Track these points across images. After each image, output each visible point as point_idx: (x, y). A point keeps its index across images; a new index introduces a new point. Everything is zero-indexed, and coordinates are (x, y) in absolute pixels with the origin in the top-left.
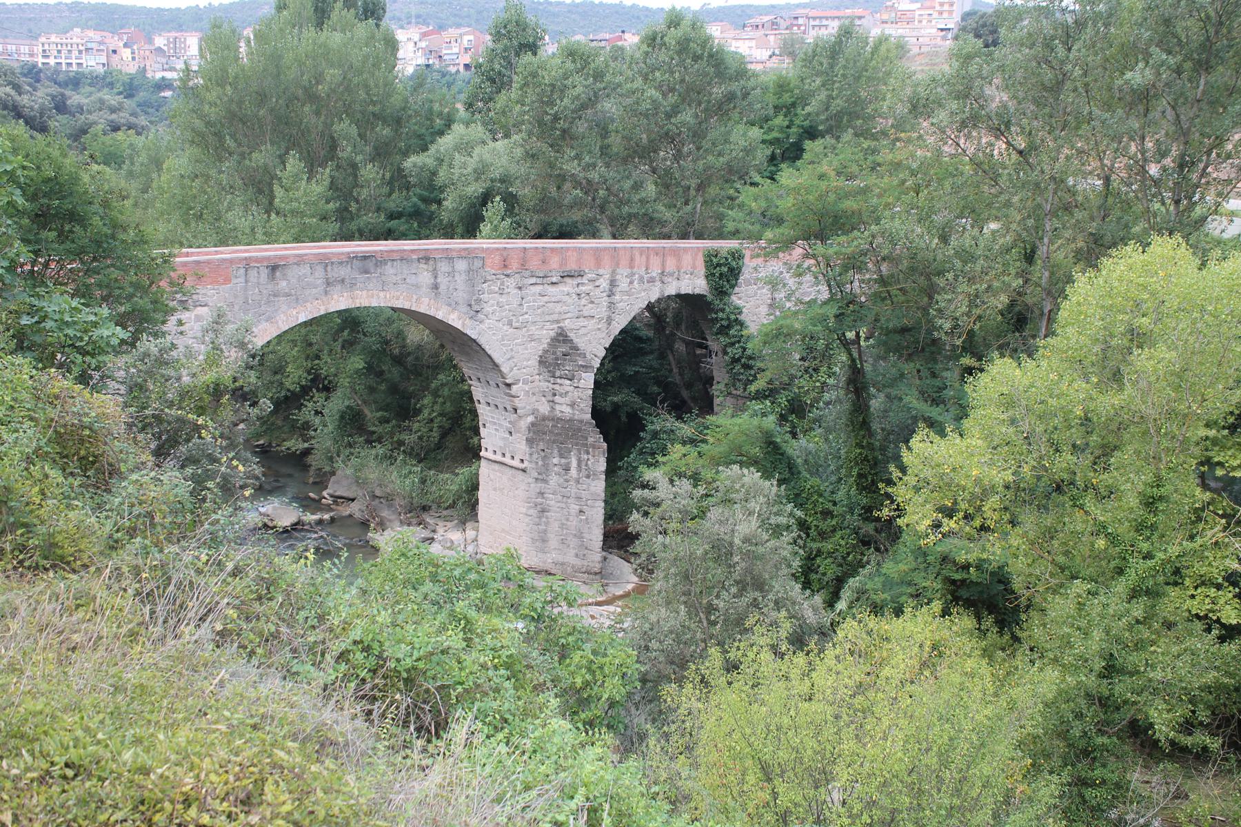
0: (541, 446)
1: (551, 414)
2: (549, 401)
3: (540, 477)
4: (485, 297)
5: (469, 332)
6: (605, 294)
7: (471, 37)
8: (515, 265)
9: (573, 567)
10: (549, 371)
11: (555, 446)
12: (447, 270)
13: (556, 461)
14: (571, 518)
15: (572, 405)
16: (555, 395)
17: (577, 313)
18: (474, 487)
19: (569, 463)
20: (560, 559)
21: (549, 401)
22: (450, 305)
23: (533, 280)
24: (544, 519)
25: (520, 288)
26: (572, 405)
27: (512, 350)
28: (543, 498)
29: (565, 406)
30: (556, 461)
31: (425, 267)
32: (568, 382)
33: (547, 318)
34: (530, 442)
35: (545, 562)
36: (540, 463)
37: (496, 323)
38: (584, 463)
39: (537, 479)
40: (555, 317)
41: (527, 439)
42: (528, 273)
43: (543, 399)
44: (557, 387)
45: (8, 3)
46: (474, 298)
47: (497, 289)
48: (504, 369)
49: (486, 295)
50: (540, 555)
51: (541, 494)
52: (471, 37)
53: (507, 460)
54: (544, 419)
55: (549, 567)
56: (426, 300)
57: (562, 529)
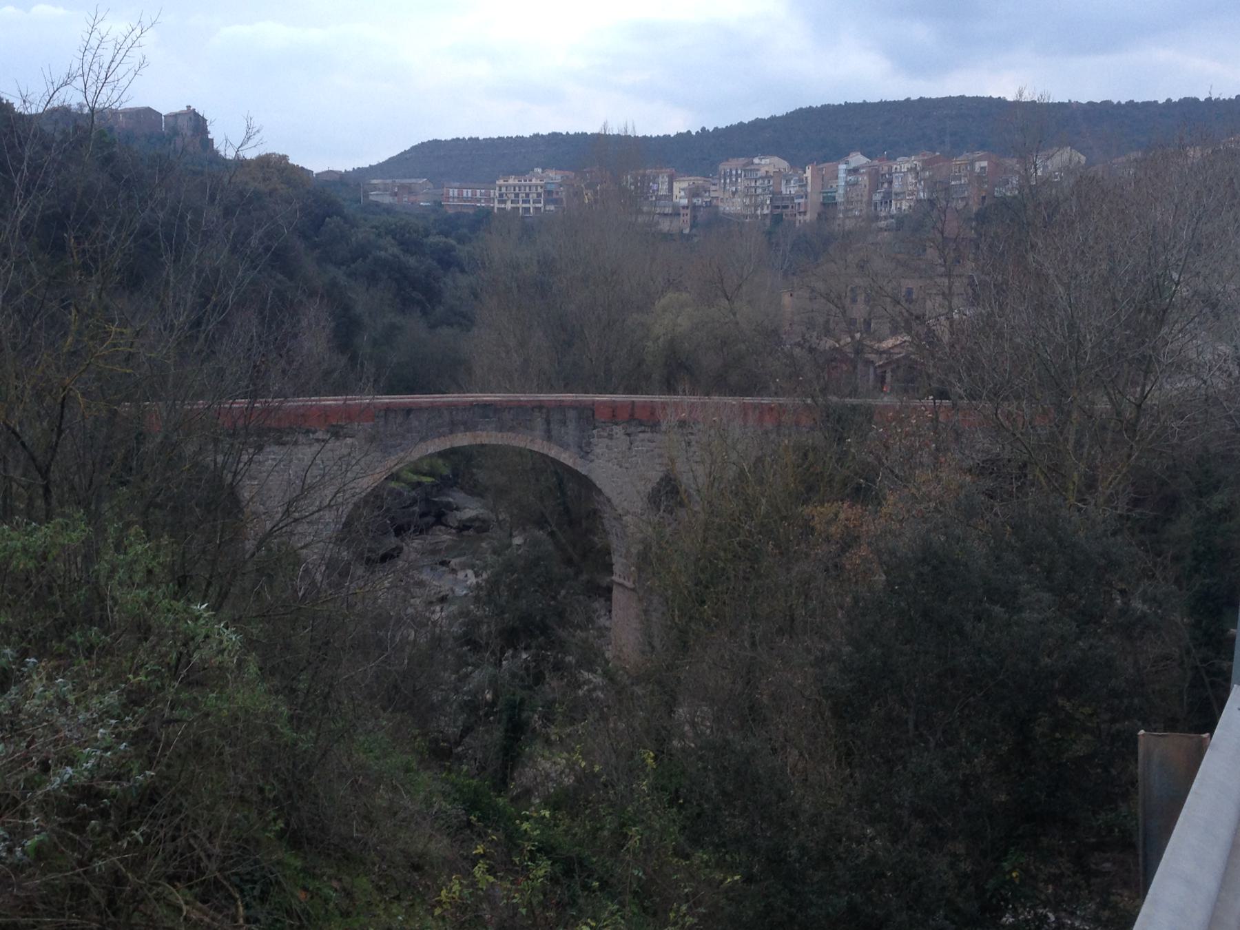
5: (579, 469)
7: (984, 164)
45: (481, 138)
49: (596, 439)
52: (984, 164)
56: (539, 441)
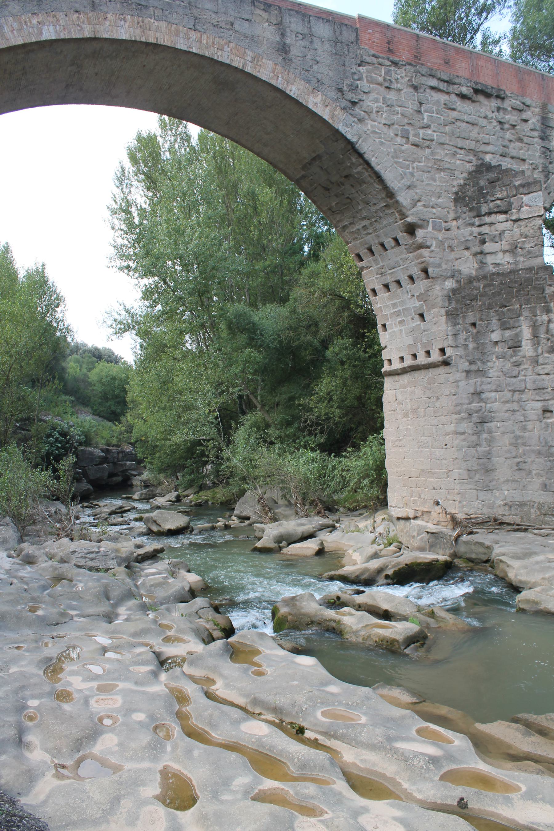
0: (471, 317)
1: (481, 273)
2: (475, 255)
3: (473, 367)
4: (364, 85)
6: (536, 134)
8: (405, 55)
9: (540, 506)
10: (471, 210)
11: (492, 313)
12: (299, 29)
13: (495, 336)
14: (530, 426)
15: (513, 250)
16: (483, 242)
17: (501, 150)
18: (380, 468)
19: (517, 335)
20: (517, 497)
21: (475, 255)
22: (308, 82)
23: (434, 82)
24: (485, 436)
25: (416, 88)
26: (513, 250)
27: (412, 174)
28: (481, 400)
29: (500, 255)
30: (495, 336)
31: (265, 15)
32: (502, 217)
33: (460, 143)
34: (451, 315)
35: (491, 506)
36: (471, 346)
37: (385, 129)
38: (543, 329)
39: (468, 372)
40: (471, 145)
41: (449, 314)
42: (424, 70)
43: (467, 253)
44: (485, 229)
46: (347, 82)
47: (380, 79)
48: (404, 198)
50: (483, 495)
51: (477, 394)
53: (422, 359)
54: (470, 280)
55: (500, 512)
56: (270, 64)
57: (516, 445)
